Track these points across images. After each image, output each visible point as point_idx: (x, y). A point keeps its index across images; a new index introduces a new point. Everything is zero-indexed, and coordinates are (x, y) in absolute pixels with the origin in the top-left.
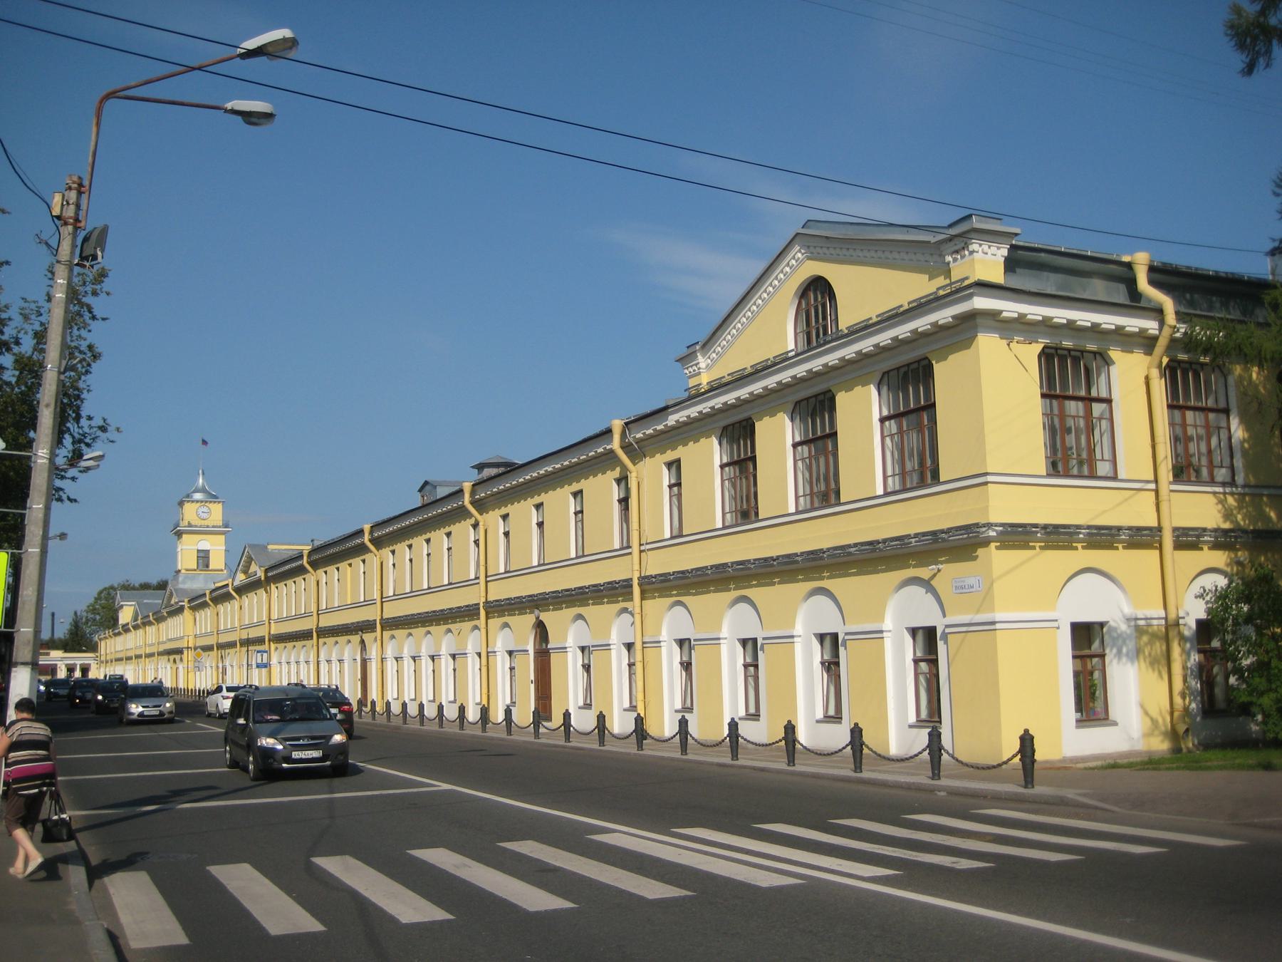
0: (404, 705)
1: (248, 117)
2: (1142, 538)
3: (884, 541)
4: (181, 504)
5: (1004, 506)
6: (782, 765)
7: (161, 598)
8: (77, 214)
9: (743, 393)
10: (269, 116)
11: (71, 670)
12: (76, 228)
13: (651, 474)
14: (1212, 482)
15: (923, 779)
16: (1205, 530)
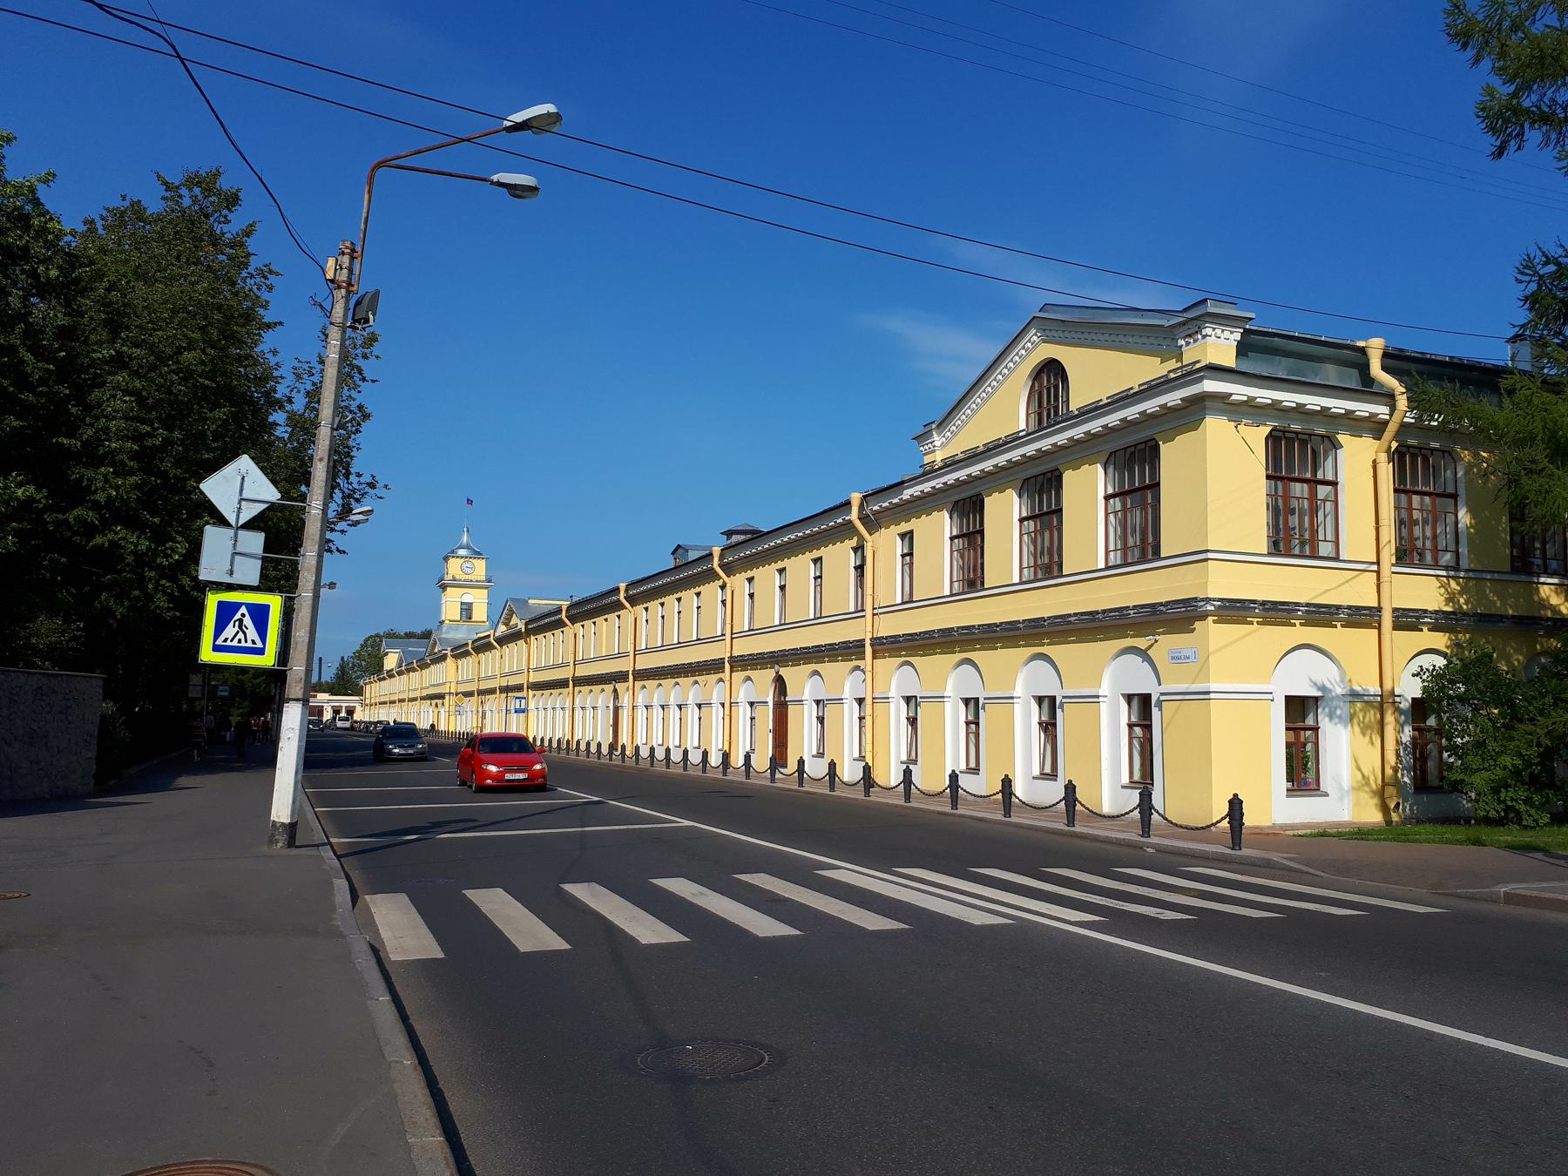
0: (652, 750)
1: (513, 189)
2: (1361, 617)
3: (1104, 611)
4: (446, 559)
5: (1222, 583)
6: (998, 816)
7: (425, 647)
8: (350, 278)
9: (974, 470)
10: (534, 189)
11: (336, 711)
12: (348, 292)
13: (885, 544)
14: (1436, 566)
15: (1133, 836)
16: (1425, 611)
